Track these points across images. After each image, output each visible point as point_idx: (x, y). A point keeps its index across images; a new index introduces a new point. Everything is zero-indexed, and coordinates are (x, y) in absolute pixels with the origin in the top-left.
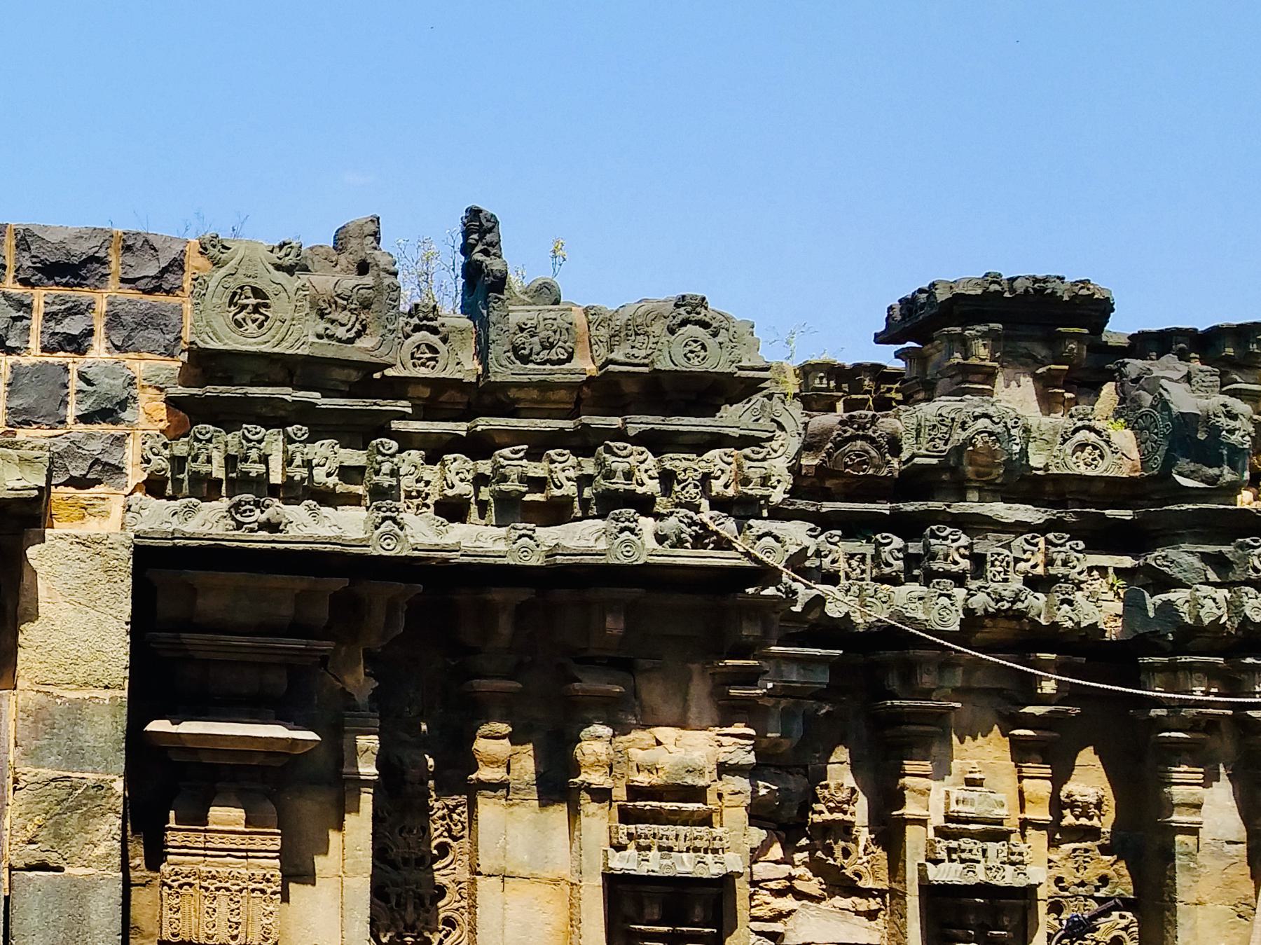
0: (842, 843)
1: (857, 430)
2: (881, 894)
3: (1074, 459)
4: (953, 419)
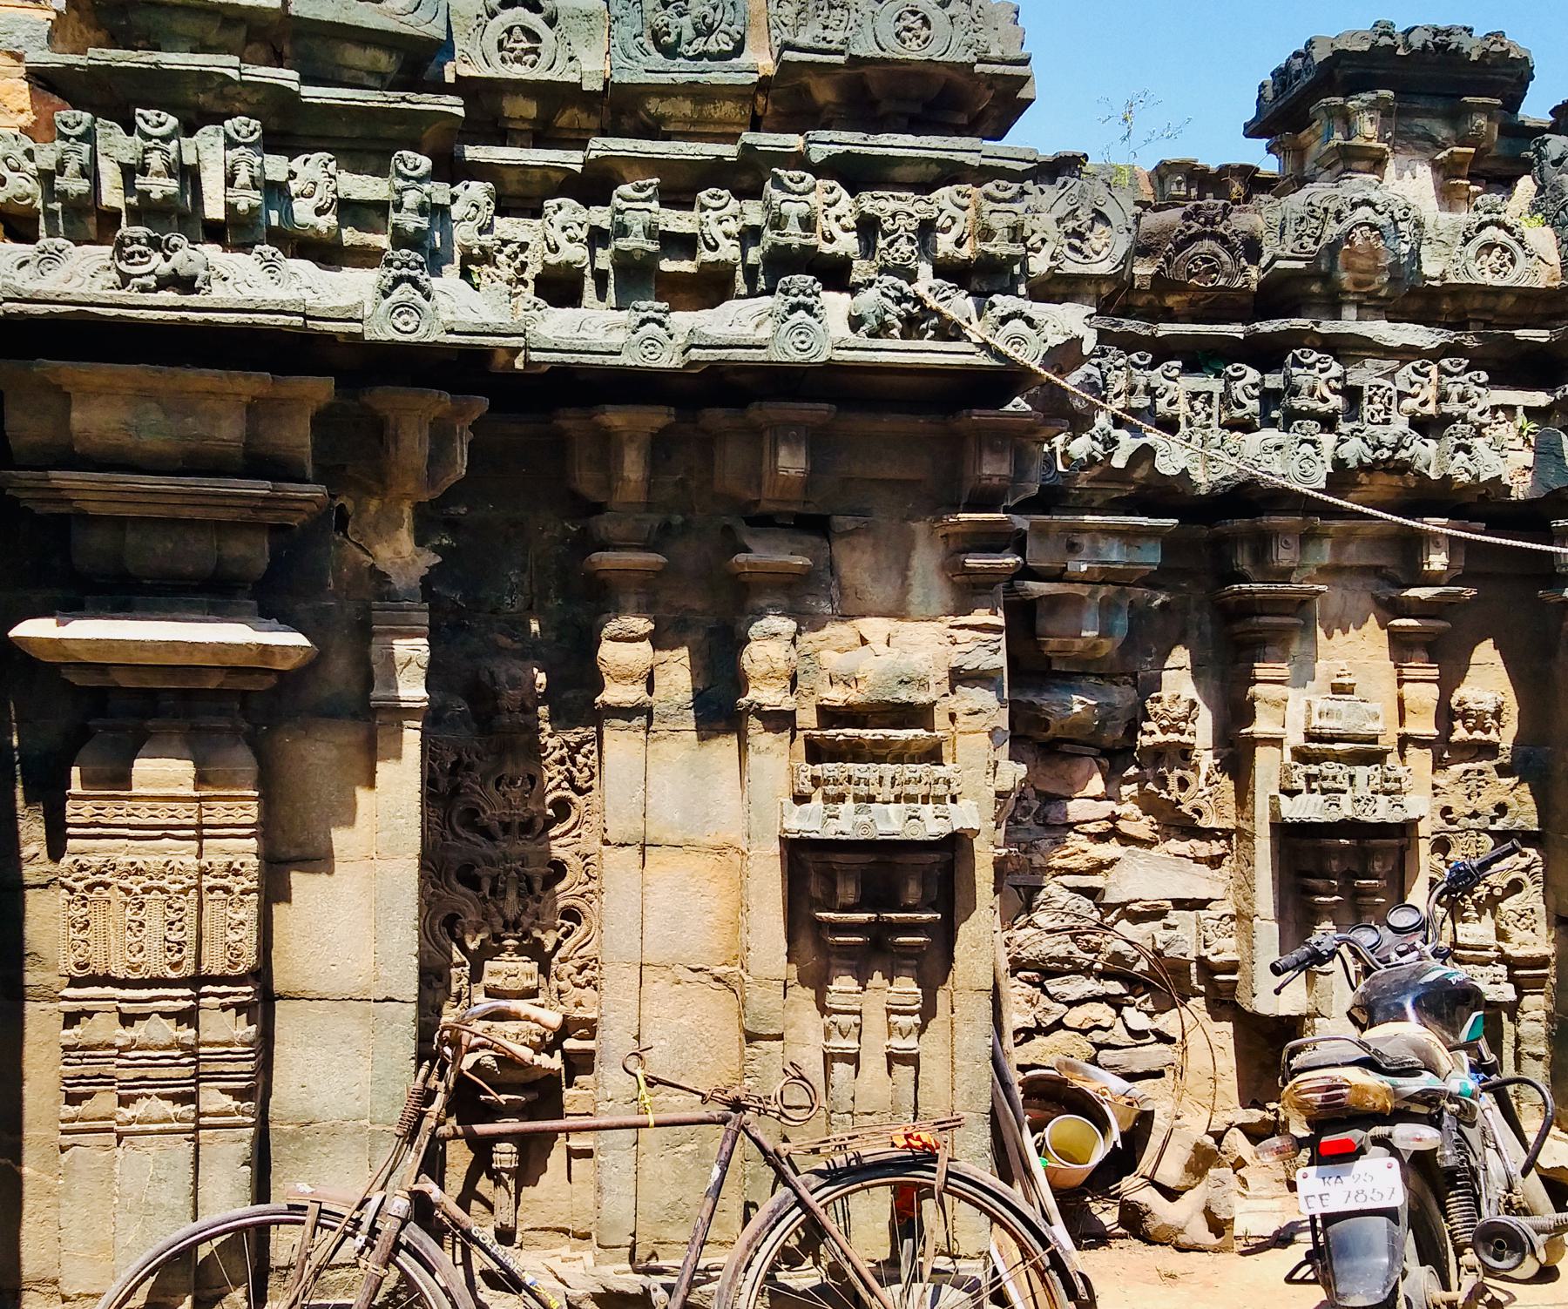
0: (1178, 772)
1: (1204, 225)
2: (1227, 834)
3: (1478, 265)
4: (1326, 210)
